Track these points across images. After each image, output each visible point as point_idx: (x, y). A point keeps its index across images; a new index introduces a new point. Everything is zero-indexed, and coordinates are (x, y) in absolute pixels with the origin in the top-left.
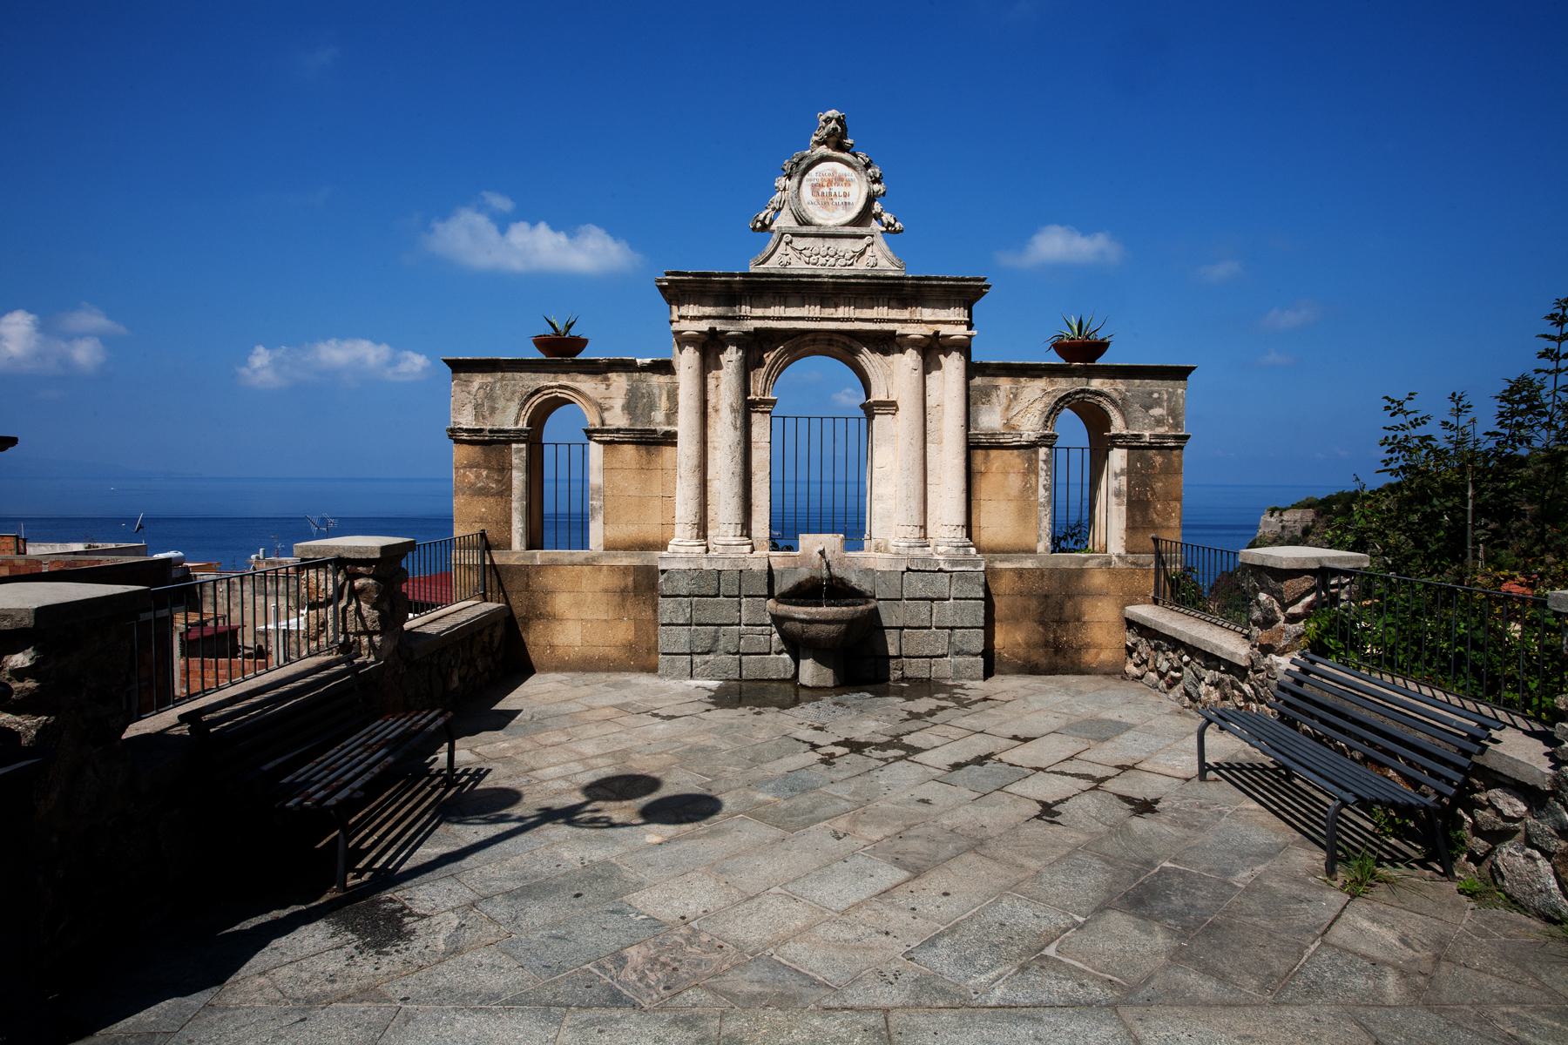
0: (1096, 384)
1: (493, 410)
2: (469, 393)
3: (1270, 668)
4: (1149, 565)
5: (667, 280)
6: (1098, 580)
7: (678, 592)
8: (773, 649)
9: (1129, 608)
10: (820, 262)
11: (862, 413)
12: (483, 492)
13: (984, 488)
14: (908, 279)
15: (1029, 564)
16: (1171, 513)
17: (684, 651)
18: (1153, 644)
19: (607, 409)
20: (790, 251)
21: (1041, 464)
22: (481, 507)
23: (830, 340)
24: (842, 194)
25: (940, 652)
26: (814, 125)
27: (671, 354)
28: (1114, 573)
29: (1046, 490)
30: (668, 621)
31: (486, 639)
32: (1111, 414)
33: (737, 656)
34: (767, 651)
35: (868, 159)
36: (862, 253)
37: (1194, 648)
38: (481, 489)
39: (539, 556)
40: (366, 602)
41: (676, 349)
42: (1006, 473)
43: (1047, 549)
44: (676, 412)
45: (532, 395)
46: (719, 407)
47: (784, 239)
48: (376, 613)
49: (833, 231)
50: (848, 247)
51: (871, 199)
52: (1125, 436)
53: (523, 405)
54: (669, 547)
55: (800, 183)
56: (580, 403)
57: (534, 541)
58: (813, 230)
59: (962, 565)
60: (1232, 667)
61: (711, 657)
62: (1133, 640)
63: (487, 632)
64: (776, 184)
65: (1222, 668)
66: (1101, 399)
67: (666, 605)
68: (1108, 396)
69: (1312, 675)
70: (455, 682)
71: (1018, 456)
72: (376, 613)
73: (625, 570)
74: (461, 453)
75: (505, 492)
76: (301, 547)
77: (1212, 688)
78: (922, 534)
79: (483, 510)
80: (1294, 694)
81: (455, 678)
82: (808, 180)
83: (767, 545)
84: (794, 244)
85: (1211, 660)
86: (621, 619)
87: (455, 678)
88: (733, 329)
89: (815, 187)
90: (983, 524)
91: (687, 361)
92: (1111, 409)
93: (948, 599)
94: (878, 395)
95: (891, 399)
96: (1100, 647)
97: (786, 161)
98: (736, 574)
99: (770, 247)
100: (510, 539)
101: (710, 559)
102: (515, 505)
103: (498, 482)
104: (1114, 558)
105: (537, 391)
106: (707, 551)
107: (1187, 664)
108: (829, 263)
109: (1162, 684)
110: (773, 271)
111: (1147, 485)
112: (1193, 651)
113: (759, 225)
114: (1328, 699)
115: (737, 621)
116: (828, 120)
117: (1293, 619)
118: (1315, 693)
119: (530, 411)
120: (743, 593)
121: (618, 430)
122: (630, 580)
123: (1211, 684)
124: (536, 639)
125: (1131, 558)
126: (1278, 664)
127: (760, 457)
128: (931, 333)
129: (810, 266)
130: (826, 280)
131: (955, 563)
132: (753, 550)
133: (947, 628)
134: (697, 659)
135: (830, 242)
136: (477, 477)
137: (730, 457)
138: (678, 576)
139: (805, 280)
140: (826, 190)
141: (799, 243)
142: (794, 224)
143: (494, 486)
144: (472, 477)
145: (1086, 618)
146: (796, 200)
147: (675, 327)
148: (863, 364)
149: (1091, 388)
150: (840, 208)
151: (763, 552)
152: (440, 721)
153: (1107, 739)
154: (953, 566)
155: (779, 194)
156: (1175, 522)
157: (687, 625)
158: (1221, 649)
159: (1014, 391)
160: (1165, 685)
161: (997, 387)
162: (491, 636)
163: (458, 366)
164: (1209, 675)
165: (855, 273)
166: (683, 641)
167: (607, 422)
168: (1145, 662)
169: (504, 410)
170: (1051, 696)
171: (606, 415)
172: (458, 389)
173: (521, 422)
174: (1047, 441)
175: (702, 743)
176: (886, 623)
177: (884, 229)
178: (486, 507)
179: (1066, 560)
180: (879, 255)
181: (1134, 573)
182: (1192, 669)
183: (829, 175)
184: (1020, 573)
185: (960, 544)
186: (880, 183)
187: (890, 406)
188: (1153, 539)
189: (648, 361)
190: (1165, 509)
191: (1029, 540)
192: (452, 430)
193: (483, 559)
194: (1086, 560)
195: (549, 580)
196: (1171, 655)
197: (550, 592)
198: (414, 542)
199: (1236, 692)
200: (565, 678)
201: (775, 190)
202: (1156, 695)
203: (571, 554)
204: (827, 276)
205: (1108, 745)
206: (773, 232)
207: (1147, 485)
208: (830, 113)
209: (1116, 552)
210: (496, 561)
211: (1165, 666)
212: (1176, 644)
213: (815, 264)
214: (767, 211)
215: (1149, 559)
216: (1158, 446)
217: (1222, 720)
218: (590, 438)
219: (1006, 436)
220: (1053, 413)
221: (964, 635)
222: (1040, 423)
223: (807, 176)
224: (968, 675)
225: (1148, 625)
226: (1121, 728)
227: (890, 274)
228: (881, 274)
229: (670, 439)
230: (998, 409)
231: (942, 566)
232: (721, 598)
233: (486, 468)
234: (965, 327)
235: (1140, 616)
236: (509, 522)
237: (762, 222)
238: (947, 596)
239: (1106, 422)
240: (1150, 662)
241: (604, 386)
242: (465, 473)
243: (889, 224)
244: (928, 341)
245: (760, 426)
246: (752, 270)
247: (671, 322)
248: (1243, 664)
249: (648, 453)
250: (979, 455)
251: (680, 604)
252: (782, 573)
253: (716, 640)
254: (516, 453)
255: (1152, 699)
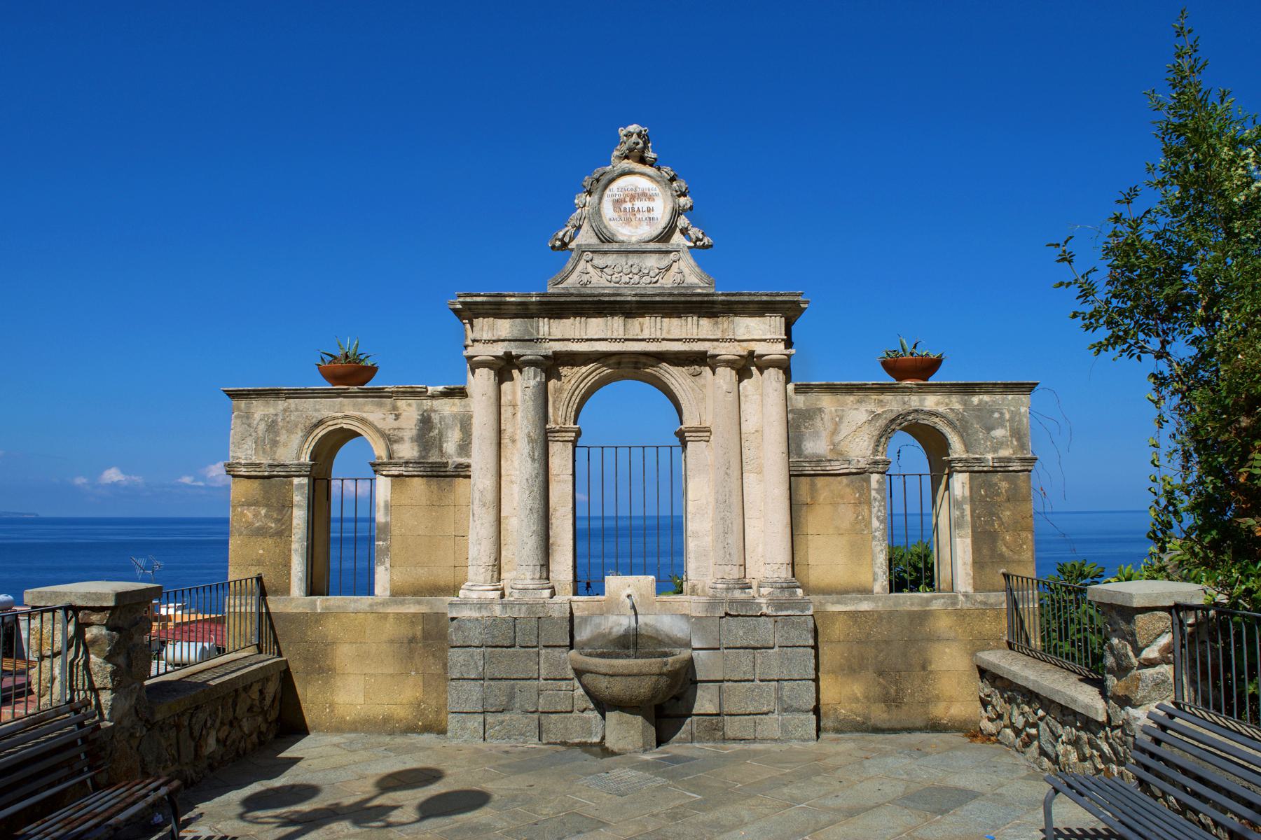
0: (931, 402)
1: (275, 443)
2: (249, 425)
3: (1127, 723)
4: (1001, 604)
5: (462, 303)
6: (943, 624)
7: (469, 643)
8: (575, 708)
9: (980, 654)
10: (623, 281)
11: (676, 441)
12: (261, 532)
13: (814, 522)
14: (718, 296)
15: (865, 606)
16: (1021, 546)
17: (477, 709)
18: (1006, 696)
19: (396, 441)
20: (590, 269)
21: (873, 493)
22: (262, 548)
23: (636, 363)
24: (645, 209)
25: (765, 709)
26: (616, 141)
27: (465, 380)
28: (961, 615)
29: (881, 522)
30: (458, 676)
31: (256, 696)
32: (949, 437)
33: (536, 716)
34: (569, 709)
35: (672, 173)
36: (669, 268)
37: (1049, 700)
38: (259, 529)
39: (320, 602)
40: (98, 656)
41: (470, 374)
42: (835, 505)
43: (883, 588)
44: (470, 443)
45: (316, 426)
46: (517, 437)
47: (584, 257)
48: (109, 667)
49: (636, 247)
50: (652, 262)
51: (676, 213)
52: (966, 460)
53: (306, 436)
54: (461, 592)
55: (601, 199)
56: (369, 435)
57: (314, 588)
58: (615, 246)
59: (787, 609)
60: (1089, 724)
61: (506, 717)
62: (987, 691)
63: (256, 688)
64: (576, 201)
65: (1078, 724)
66: (937, 420)
67: (456, 656)
68: (943, 417)
69: (1169, 732)
70: (211, 745)
71: (848, 485)
72: (109, 667)
73: (413, 619)
74: (240, 490)
75: (283, 533)
76: (32, 593)
77: (1069, 747)
78: (544, 575)
79: (261, 552)
80: (1152, 755)
81: (212, 741)
82: (609, 196)
83: (570, 588)
84: (596, 262)
85: (1066, 714)
86: (408, 674)
87: (212, 741)
88: (529, 352)
89: (618, 203)
90: (812, 561)
91: (480, 383)
92: (947, 430)
93: (773, 648)
94: (690, 421)
95: (703, 425)
96: (951, 700)
97: (586, 177)
98: (534, 623)
99: (569, 266)
100: (289, 584)
101: (504, 606)
102: (295, 546)
103: (278, 521)
104: (961, 597)
105: (321, 422)
106: (503, 596)
107: (1041, 719)
108: (632, 281)
109: (1018, 742)
110: (572, 291)
111: (994, 514)
112: (1048, 704)
113: (558, 243)
114: (1188, 761)
115: (536, 676)
116: (629, 135)
117: (1151, 663)
118: (1175, 755)
119: (313, 444)
120: (542, 643)
121: (407, 463)
122: (418, 630)
123: (1069, 742)
124: (310, 696)
125: (980, 597)
126: (1136, 719)
127: (561, 492)
128: (745, 353)
129: (612, 284)
130: (629, 299)
131: (779, 606)
132: (553, 595)
133: (774, 680)
134: (490, 719)
135: (633, 259)
136: (255, 516)
137: (528, 492)
138: (470, 625)
139: (607, 299)
140: (628, 205)
141: (600, 261)
142: (594, 241)
143: (273, 525)
144: (250, 515)
145: (933, 667)
146: (596, 217)
147: (470, 351)
148: (672, 387)
149: (925, 409)
150: (644, 223)
151: (565, 596)
152: (163, 791)
153: (947, 811)
154: (776, 610)
155: (579, 211)
156: (1027, 555)
157: (480, 679)
158: (1075, 701)
159: (839, 413)
160: (1021, 744)
161: (820, 410)
162: (261, 692)
163: (234, 395)
164: (1066, 733)
165: (658, 291)
166: (475, 698)
167: (396, 455)
168: (1000, 717)
169: (285, 445)
170: (890, 760)
171: (395, 447)
172: (239, 421)
173: (303, 455)
174: (882, 467)
175: (476, 820)
176: (698, 678)
177: (692, 244)
178: (263, 549)
179: (909, 600)
180: (686, 271)
181: (984, 614)
182: (1047, 724)
183: (632, 190)
184: (854, 616)
185: (785, 585)
186: (685, 196)
187: (703, 431)
188: (1004, 575)
189: (440, 388)
190: (1015, 541)
191: (864, 578)
192: (229, 465)
193: (259, 606)
194: (928, 601)
195: (331, 628)
196: (1026, 708)
197: (332, 644)
198: (160, 589)
199: (1095, 753)
200: (343, 740)
201: (574, 208)
202: (1013, 756)
203: (355, 601)
204: (630, 295)
205: (949, 818)
206: (572, 250)
207: (994, 514)
208: (634, 128)
209: (963, 590)
210: (272, 608)
211: (1019, 721)
212: (1031, 696)
213: (618, 283)
214: (566, 229)
215: (1000, 599)
216: (1002, 468)
217: (1078, 791)
218: (375, 471)
219: (833, 463)
220: (886, 433)
221: (792, 689)
222: (871, 447)
223: (607, 192)
224: (798, 735)
225: (1000, 673)
226: (965, 796)
227: (699, 291)
228: (689, 292)
229: (462, 472)
230: (824, 434)
231: (765, 610)
232: (517, 649)
233: (266, 506)
234: (782, 346)
235: (989, 662)
236: (287, 565)
237: (562, 240)
238: (771, 645)
239: (944, 445)
240: (1006, 717)
241: (393, 416)
242: (242, 512)
243: (698, 239)
244: (743, 362)
245: (560, 458)
246: (550, 291)
247: (466, 347)
248: (1100, 720)
249: (440, 488)
250: (369, 481)
251: (472, 656)
252: (585, 620)
253: (511, 697)
254: (297, 489)
255: (1007, 760)
